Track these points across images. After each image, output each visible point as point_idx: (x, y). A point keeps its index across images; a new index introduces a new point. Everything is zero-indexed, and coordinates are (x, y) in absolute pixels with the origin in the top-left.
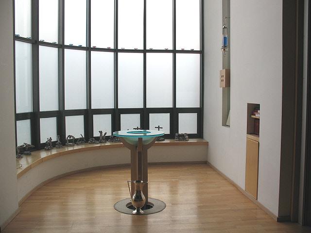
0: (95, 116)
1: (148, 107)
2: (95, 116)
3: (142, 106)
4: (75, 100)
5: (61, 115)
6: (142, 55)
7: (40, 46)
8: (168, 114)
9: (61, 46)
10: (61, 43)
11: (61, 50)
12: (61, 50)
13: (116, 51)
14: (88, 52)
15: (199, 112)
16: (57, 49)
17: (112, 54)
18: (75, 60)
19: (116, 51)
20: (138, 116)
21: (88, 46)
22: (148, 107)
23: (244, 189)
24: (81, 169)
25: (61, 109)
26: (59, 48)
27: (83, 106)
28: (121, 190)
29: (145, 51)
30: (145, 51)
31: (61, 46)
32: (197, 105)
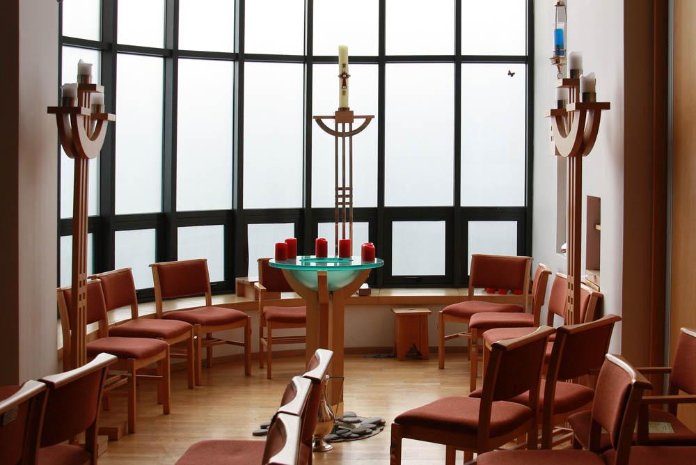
0: (251, 228)
1: (464, 204)
2: (251, 228)
3: (450, 202)
4: (204, 188)
5: (166, 224)
6: (375, 68)
7: (118, 55)
8: (441, 225)
9: (171, 54)
10: (171, 47)
11: (170, 62)
12: (170, 62)
13: (239, 57)
14: (237, 63)
15: (523, 217)
16: (161, 60)
17: (299, 68)
18: (205, 86)
19: (239, 57)
20: (440, 227)
21: (237, 51)
22: (464, 204)
23: (672, 432)
24: (222, 355)
25: (168, 209)
26: (165, 58)
27: (153, 206)
28: (185, 423)
29: (458, 59)
30: (458, 59)
31: (171, 54)
32: (520, 202)
